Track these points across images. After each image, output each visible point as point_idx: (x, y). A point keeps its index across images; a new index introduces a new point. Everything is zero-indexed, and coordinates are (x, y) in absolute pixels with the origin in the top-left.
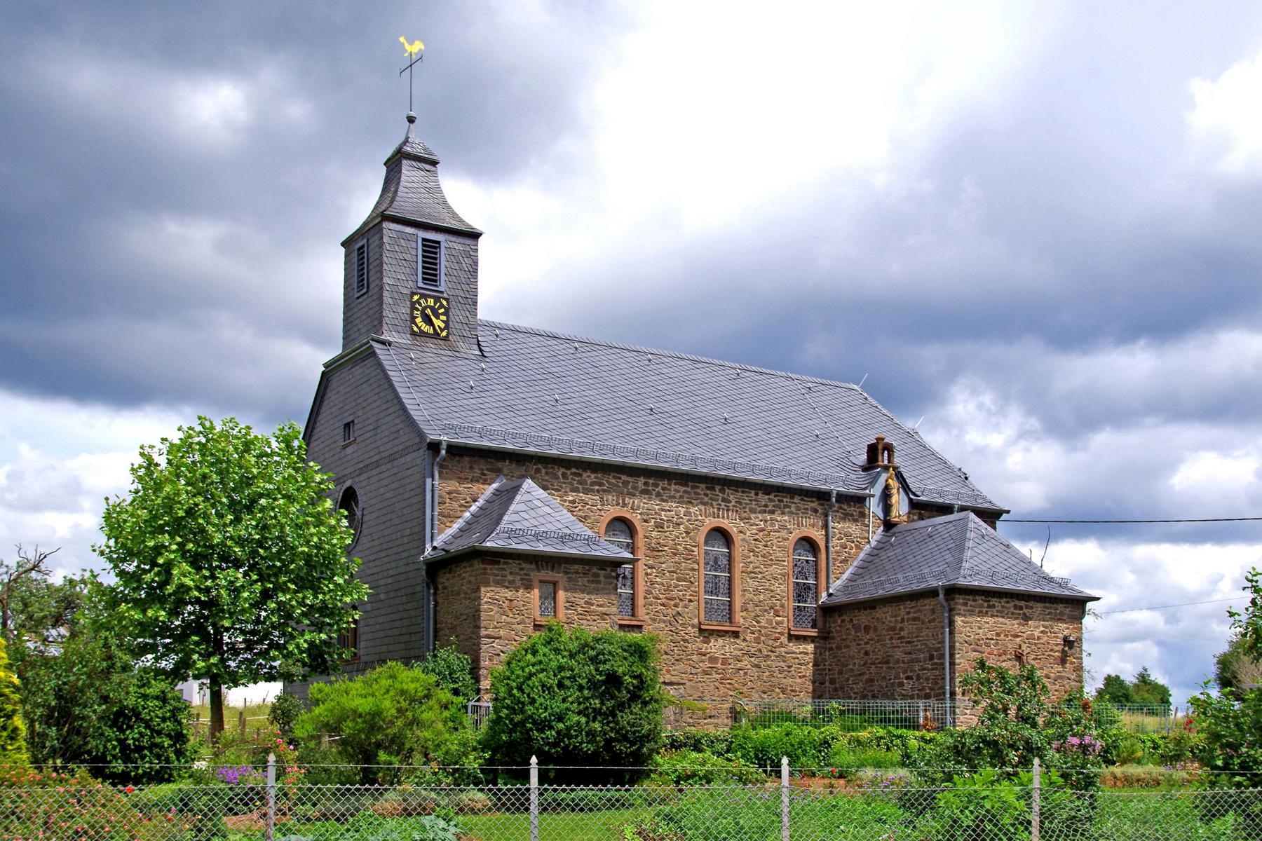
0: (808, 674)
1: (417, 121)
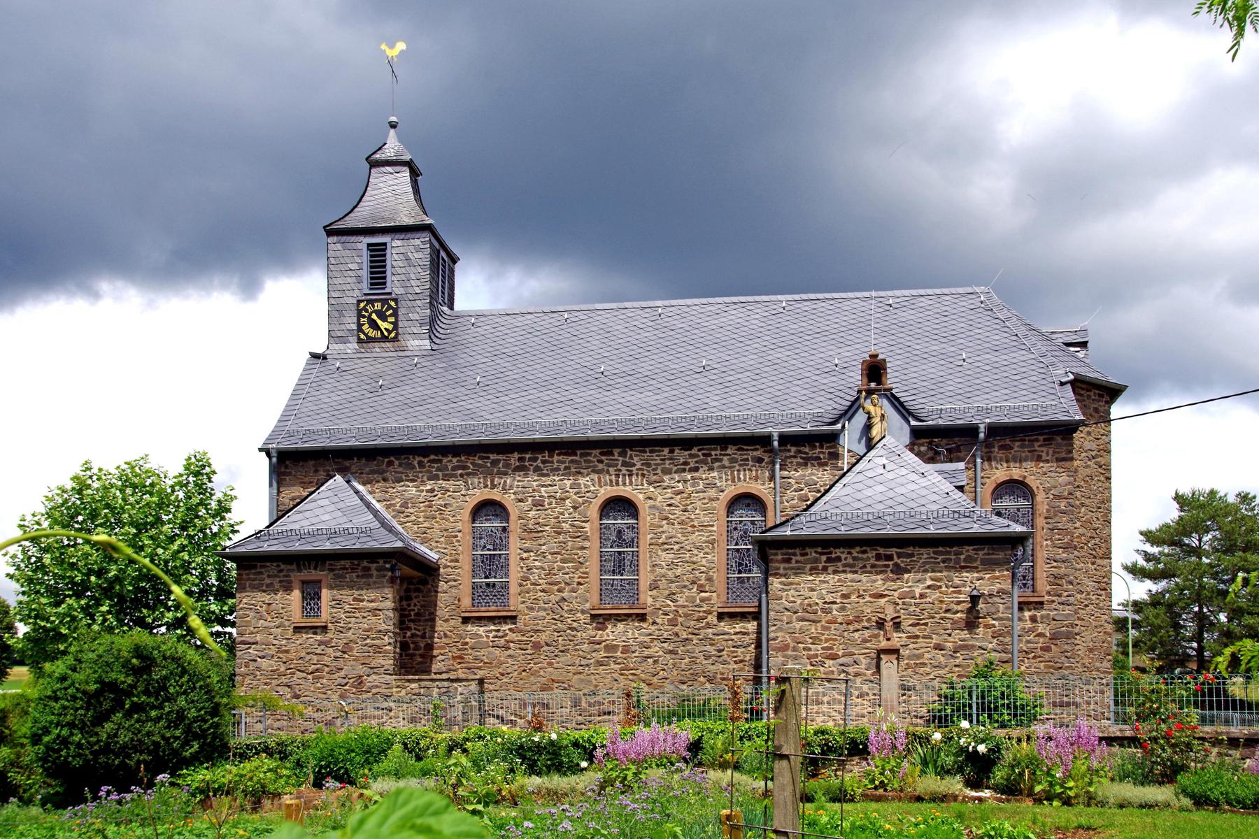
0: (747, 659)
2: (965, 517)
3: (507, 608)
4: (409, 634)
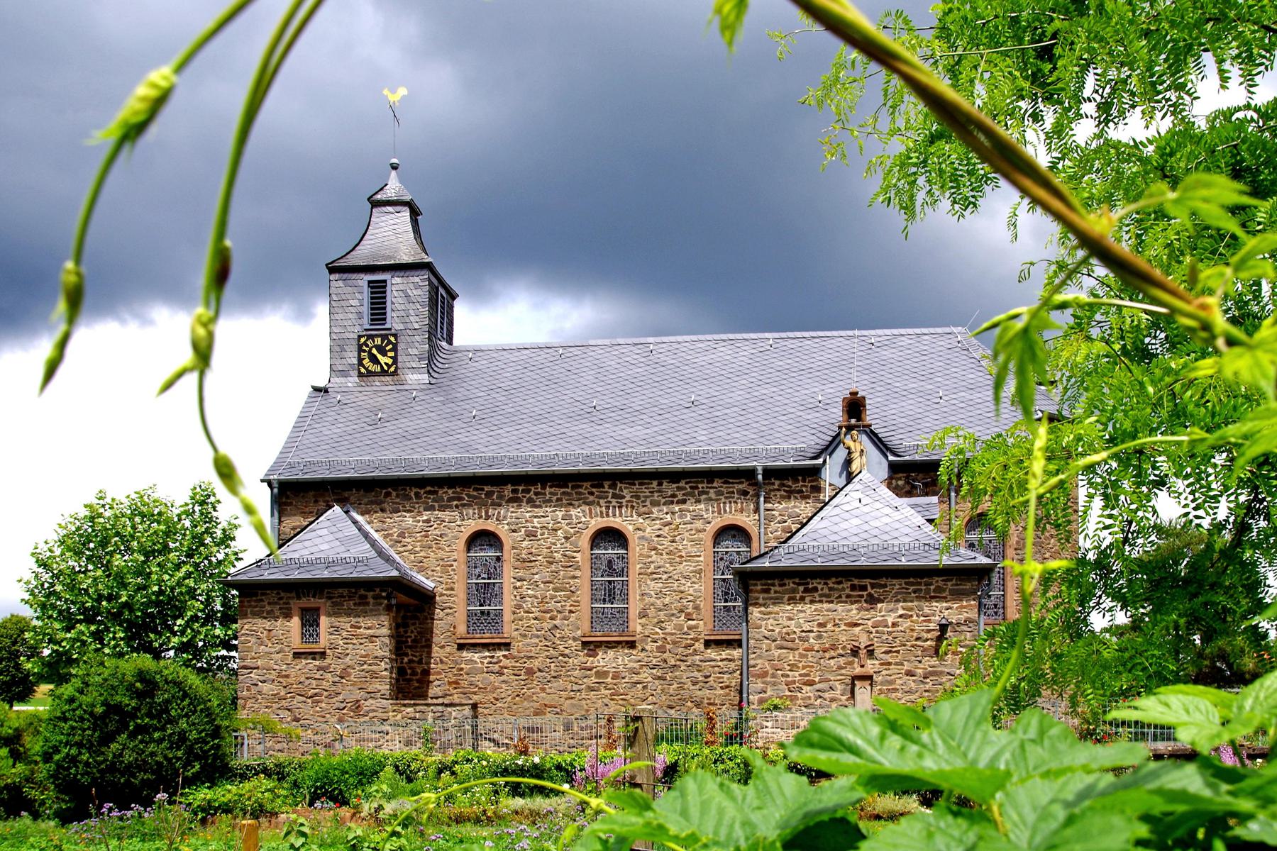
2: (935, 549)
3: (501, 635)
4: (406, 660)
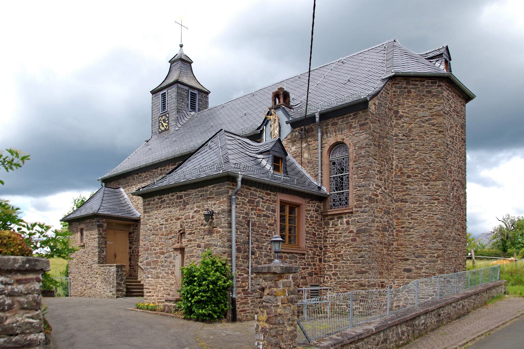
1: (189, 52)
